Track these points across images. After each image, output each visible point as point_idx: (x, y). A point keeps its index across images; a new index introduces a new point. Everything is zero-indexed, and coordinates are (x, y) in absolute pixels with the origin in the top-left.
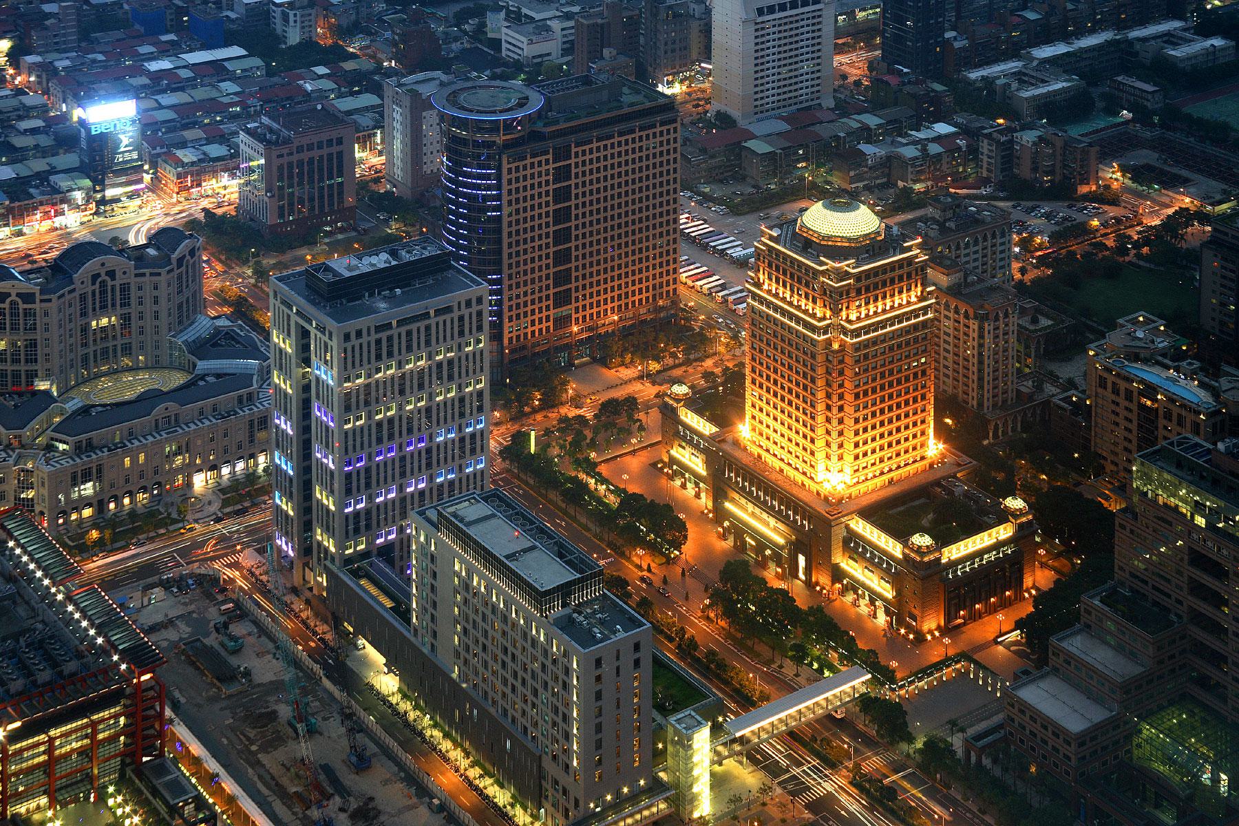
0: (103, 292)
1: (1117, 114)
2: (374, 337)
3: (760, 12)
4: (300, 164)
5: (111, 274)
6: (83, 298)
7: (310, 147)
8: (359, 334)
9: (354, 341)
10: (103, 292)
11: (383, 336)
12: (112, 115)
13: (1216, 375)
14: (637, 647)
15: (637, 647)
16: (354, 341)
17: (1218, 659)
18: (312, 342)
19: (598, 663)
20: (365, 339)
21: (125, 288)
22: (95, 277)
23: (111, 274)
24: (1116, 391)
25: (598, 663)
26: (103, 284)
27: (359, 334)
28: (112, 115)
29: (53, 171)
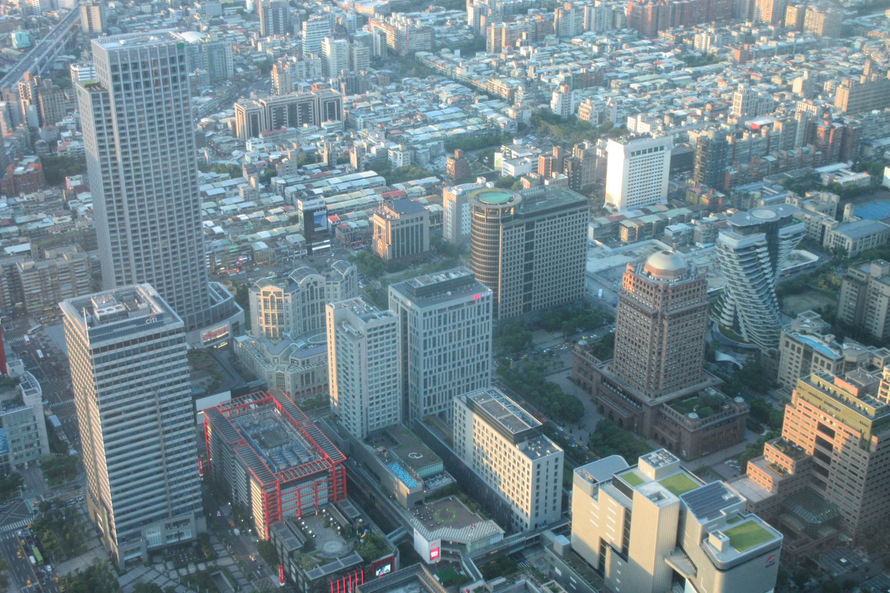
0: (312, 291)
1: (475, 181)
2: (437, 315)
3: (633, 154)
4: (407, 228)
5: (315, 283)
6: (303, 294)
7: (407, 222)
8: (430, 313)
9: (428, 317)
10: (312, 291)
11: (442, 314)
12: (713, 392)
13: (841, 342)
14: (557, 460)
15: (557, 460)
16: (428, 317)
17: (825, 473)
18: (518, 406)
19: (539, 466)
20: (433, 316)
21: (322, 290)
22: (308, 284)
23: (315, 283)
24: (793, 348)
25: (539, 466)
26: (312, 288)
27: (430, 313)
28: (713, 392)
29: (288, 233)
